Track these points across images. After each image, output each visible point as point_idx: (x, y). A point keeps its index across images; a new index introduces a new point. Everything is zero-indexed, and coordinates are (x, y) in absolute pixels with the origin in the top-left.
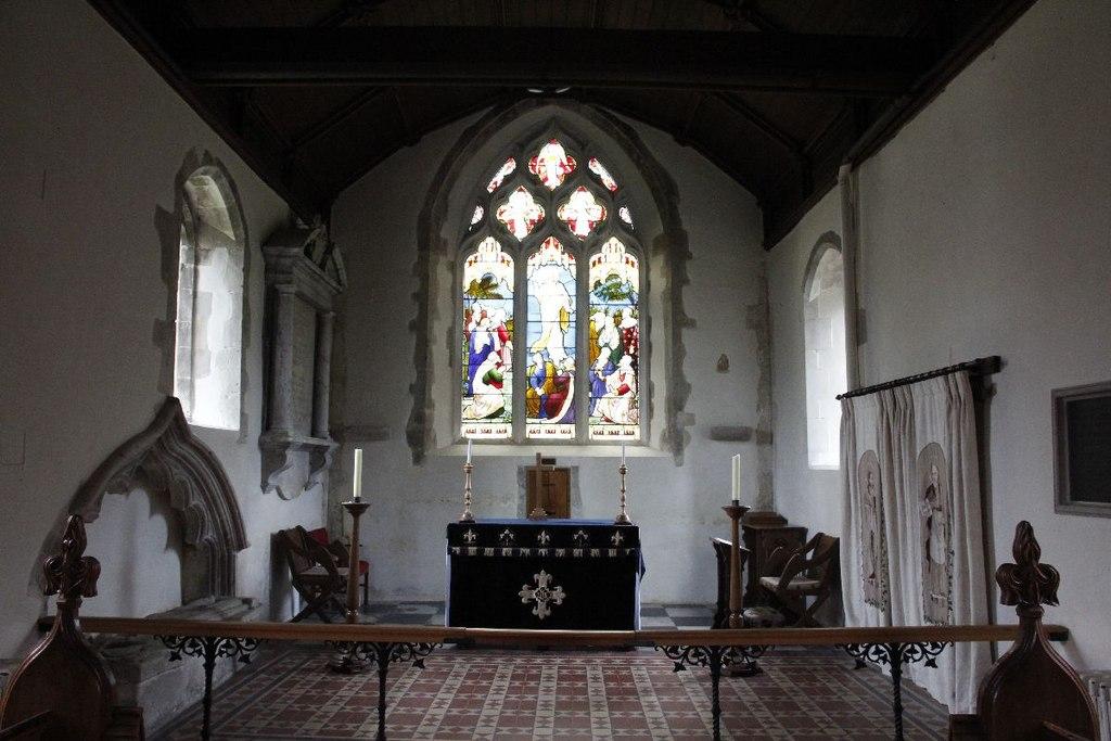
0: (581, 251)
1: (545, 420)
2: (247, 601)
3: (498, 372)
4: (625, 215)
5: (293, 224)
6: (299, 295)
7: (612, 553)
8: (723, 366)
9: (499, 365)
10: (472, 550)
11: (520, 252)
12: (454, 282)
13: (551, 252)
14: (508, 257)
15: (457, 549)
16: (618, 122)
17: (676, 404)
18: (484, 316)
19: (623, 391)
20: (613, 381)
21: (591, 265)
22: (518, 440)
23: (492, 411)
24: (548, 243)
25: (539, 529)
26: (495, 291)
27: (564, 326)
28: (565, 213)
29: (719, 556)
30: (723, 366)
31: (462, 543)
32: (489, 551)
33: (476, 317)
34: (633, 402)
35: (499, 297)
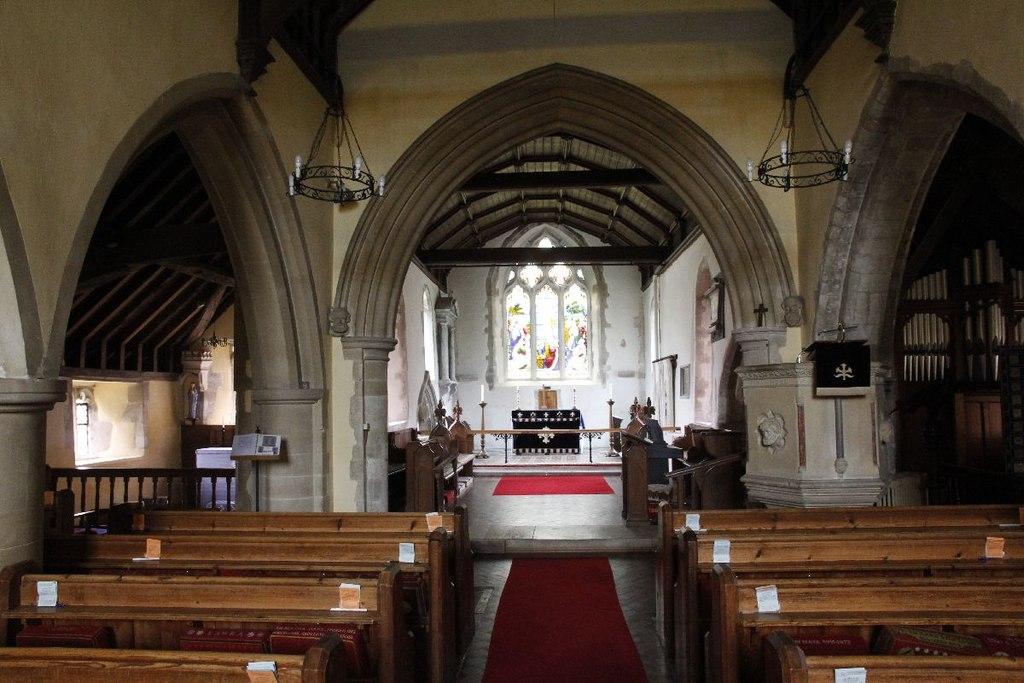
0: (559, 291)
3: (523, 348)
8: (623, 345)
10: (521, 420)
11: (532, 292)
16: (575, 233)
17: (603, 362)
25: (544, 412)
30: (623, 345)
31: (517, 417)
32: (527, 420)
33: (513, 324)
35: (522, 313)
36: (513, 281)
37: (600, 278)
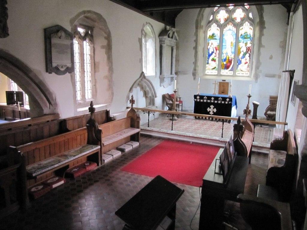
0: (238, 26)
1: (226, 70)
2: (156, 107)
3: (215, 58)
4: (251, 15)
5: (165, 28)
6: (167, 45)
7: (227, 103)
9: (215, 56)
11: (221, 27)
12: (205, 36)
13: (230, 27)
14: (219, 28)
15: (196, 100)
17: (257, 68)
18: (212, 44)
19: (246, 63)
20: (243, 61)
21: (240, 30)
22: (219, 75)
23: (213, 68)
24: (229, 24)
26: (215, 38)
27: (232, 47)
28: (234, 16)
29: (254, 106)
30: (271, 58)
32: (202, 101)
33: (210, 44)
34: (248, 66)
36: (212, 20)
37: (261, 17)
